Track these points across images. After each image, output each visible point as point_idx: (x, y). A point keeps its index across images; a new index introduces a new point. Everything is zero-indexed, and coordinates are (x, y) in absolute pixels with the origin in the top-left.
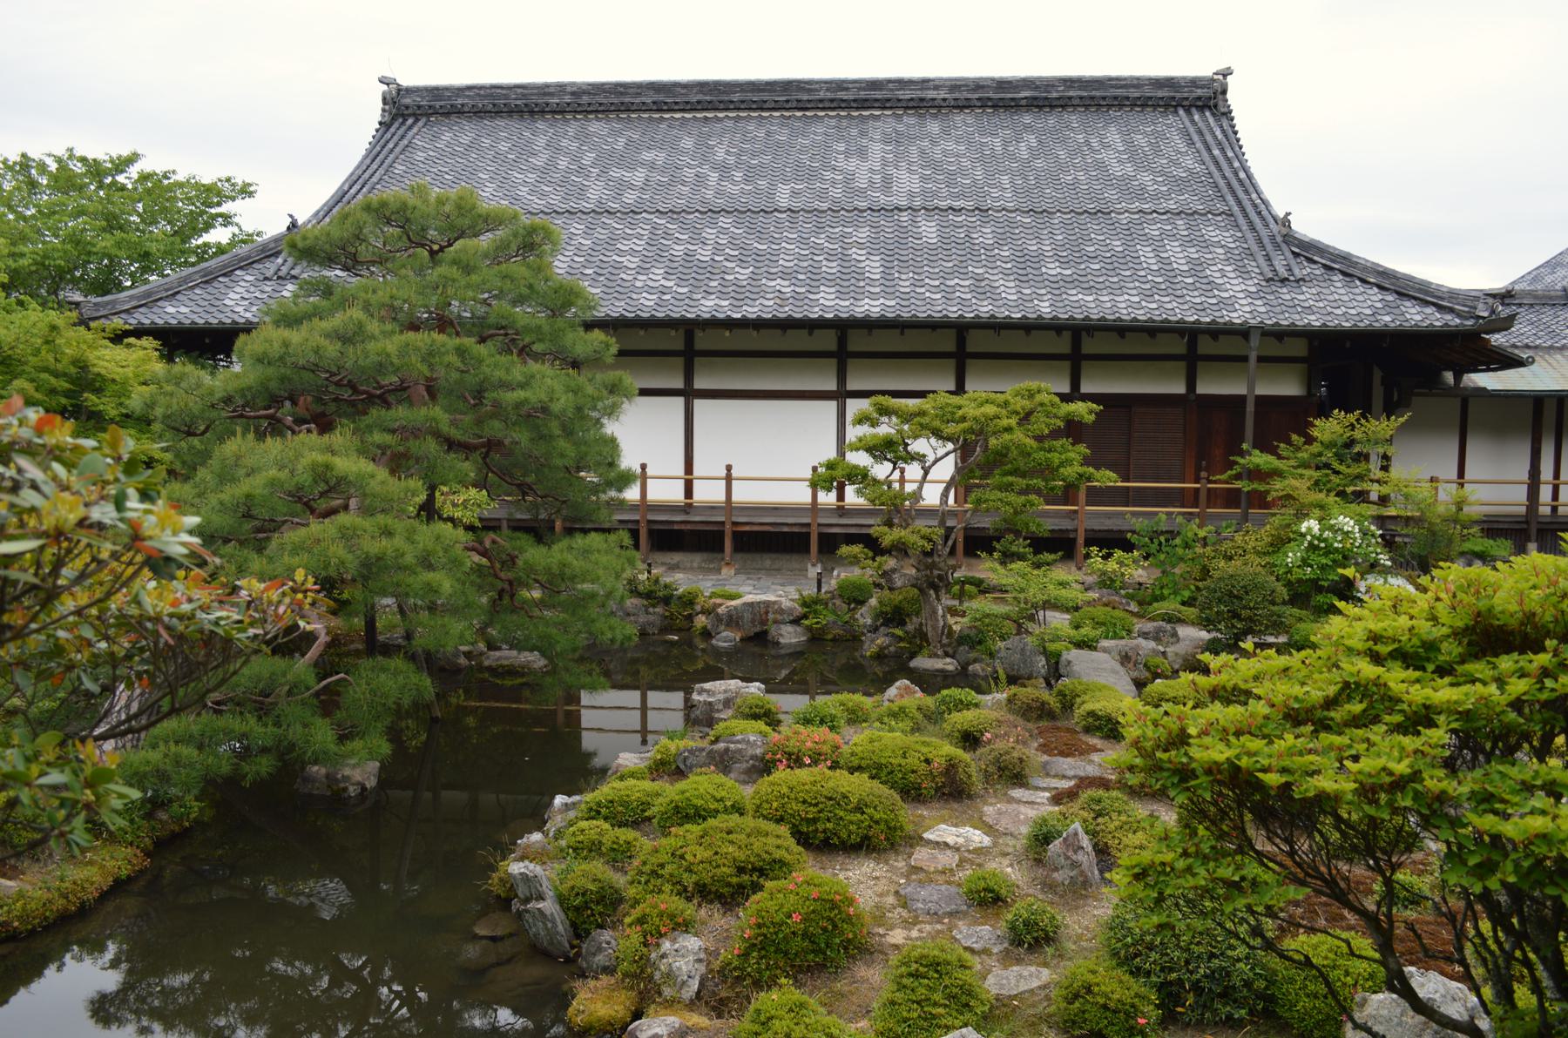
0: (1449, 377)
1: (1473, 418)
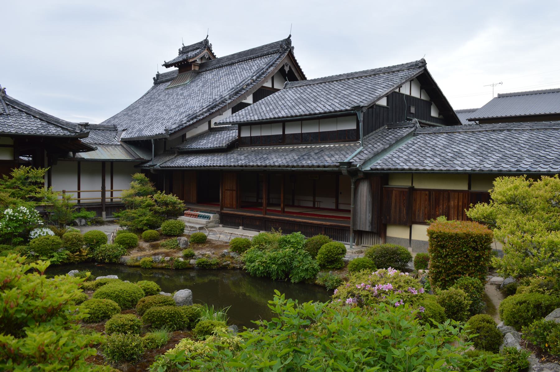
0: (71, 154)
1: (84, 169)
